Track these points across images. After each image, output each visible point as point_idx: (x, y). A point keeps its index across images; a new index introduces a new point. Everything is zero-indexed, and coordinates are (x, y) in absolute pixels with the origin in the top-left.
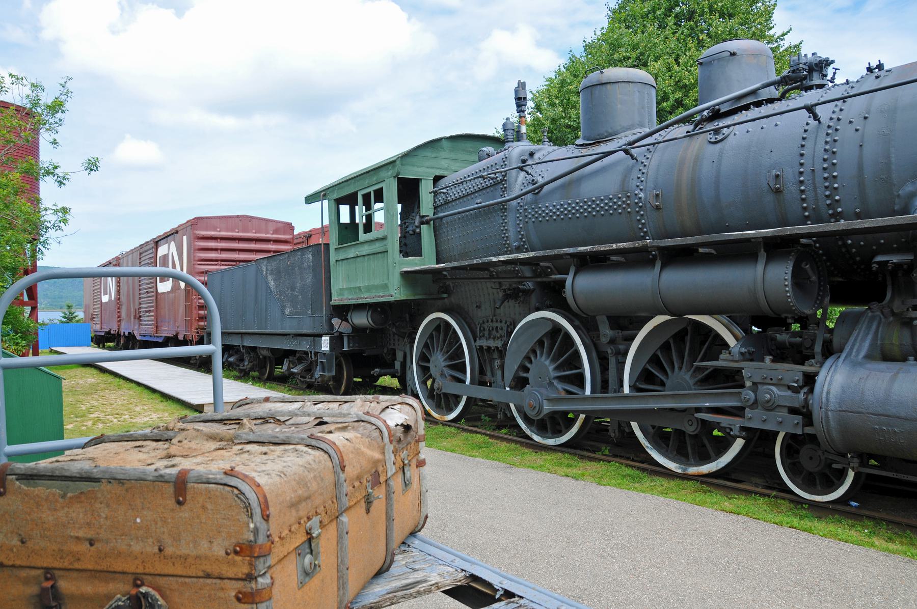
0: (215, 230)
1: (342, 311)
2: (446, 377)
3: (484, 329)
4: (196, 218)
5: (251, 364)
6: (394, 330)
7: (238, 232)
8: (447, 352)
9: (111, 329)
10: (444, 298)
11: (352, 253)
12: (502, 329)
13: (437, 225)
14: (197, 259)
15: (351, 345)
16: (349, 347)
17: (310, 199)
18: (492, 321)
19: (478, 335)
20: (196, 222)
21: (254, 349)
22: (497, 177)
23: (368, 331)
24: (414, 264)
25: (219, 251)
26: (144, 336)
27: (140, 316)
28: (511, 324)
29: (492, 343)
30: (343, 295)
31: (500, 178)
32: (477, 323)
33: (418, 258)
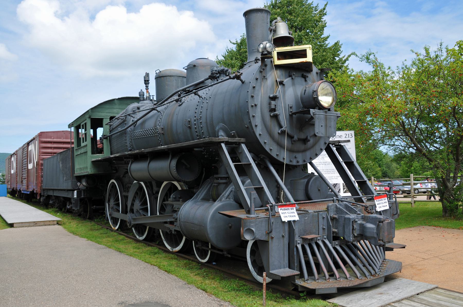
0: (51, 138)
1: (79, 178)
2: (114, 210)
4: (41, 132)
5: (59, 204)
7: (63, 139)
9: (14, 188)
14: (41, 152)
15: (85, 195)
16: (84, 195)
20: (41, 134)
21: (57, 197)
24: (99, 157)
25: (53, 149)
26: (24, 191)
27: (22, 181)
33: (101, 154)
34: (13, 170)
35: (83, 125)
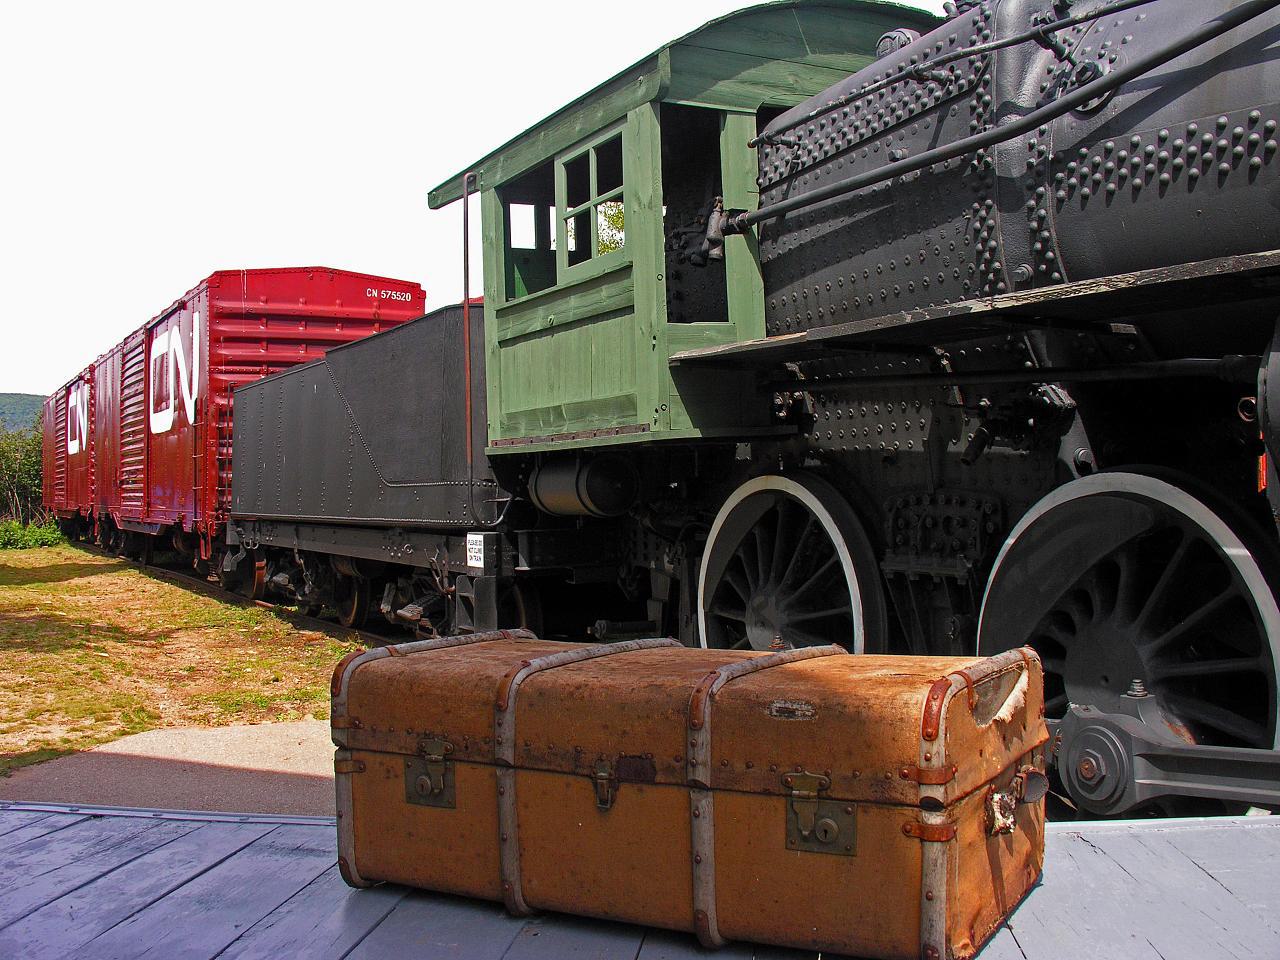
3: (907, 524)
6: (647, 522)
8: (794, 586)
10: (788, 437)
11: (537, 320)
12: (964, 523)
13: (765, 229)
15: (537, 558)
17: (439, 198)
18: (933, 501)
19: (889, 539)
20: (221, 283)
21: (322, 559)
22: (958, 78)
23: (579, 524)
24: (706, 340)
25: (265, 344)
26: (129, 522)
28: (995, 511)
29: (934, 567)
30: (516, 429)
31: (967, 77)
32: (885, 506)
34: (77, 442)
35: (578, 169)
